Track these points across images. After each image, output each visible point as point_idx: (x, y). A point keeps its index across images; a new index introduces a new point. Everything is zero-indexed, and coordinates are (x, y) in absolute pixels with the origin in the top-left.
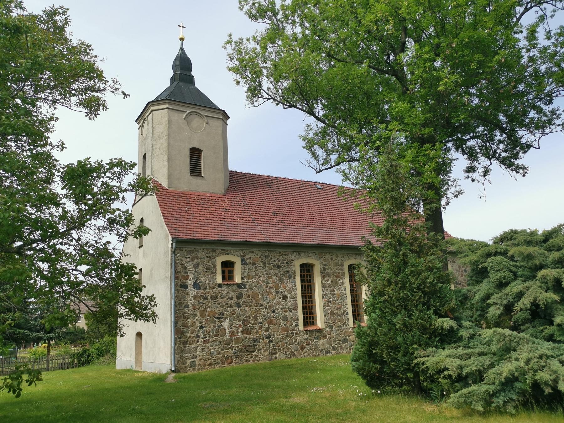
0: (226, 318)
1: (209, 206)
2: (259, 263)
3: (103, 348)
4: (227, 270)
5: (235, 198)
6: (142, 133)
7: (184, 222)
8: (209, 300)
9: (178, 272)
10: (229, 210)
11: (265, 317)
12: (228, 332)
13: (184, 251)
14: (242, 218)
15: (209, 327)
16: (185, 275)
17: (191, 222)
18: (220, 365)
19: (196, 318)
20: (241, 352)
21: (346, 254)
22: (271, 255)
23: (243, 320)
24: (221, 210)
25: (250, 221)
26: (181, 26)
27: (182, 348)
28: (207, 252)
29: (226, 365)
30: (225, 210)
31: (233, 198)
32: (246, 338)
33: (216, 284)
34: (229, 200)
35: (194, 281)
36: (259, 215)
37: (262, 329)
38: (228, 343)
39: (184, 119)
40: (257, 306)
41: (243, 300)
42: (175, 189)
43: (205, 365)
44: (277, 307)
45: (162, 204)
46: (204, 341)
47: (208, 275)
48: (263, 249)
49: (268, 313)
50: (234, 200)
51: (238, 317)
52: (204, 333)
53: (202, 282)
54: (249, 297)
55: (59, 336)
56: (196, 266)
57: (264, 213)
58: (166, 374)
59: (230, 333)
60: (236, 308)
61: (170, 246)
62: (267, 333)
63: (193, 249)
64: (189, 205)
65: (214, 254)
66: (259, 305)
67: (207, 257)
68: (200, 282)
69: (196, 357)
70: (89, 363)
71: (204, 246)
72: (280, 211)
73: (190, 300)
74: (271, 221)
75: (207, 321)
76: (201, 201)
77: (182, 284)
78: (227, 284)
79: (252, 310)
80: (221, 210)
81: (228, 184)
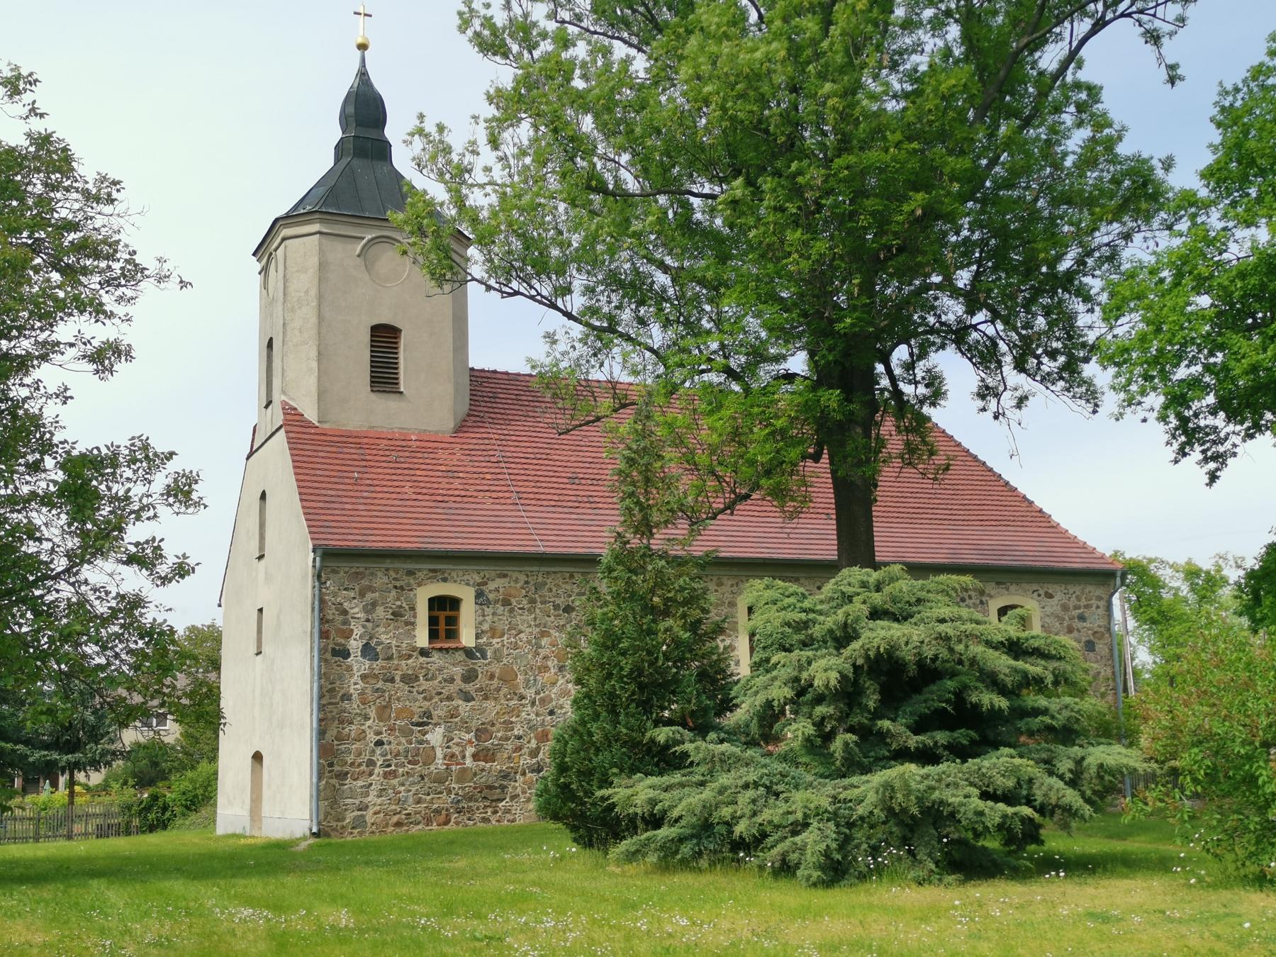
0: (436, 725)
1: (411, 466)
2: (519, 601)
3: (198, 791)
4: (442, 615)
5: (481, 441)
6: (265, 285)
7: (347, 506)
9: (328, 621)
10: (461, 475)
11: (531, 724)
12: (441, 756)
13: (342, 574)
14: (488, 494)
15: (398, 743)
16: (345, 627)
18: (420, 827)
19: (369, 723)
20: (471, 799)
21: (744, 579)
22: (548, 581)
23: (477, 730)
24: (440, 474)
26: (360, 14)
27: (334, 786)
28: (394, 576)
29: (434, 827)
30: (450, 474)
32: (483, 770)
33: (414, 649)
34: (465, 447)
35: (365, 641)
36: (533, 484)
37: (523, 751)
38: (440, 780)
39: (359, 256)
40: (511, 699)
41: (477, 684)
42: (334, 426)
43: (387, 825)
44: (560, 702)
45: (299, 464)
46: (385, 773)
47: (397, 628)
48: (531, 569)
49: (537, 715)
50: (477, 447)
51: (466, 723)
52: (386, 755)
54: (492, 677)
55: (95, 760)
56: (371, 608)
57: (547, 479)
58: (300, 839)
59: (444, 758)
60: (460, 702)
61: (310, 563)
62: (534, 760)
64: (364, 463)
65: (412, 581)
66: (516, 697)
67: (395, 587)
68: (379, 644)
69: (367, 807)
70: (165, 827)
71: (388, 564)
72: (590, 471)
73: (355, 684)
74: (562, 498)
75: (391, 729)
76: (393, 453)
77: (337, 648)
78: (441, 649)
79: (498, 707)
80: (440, 474)
81: (464, 407)
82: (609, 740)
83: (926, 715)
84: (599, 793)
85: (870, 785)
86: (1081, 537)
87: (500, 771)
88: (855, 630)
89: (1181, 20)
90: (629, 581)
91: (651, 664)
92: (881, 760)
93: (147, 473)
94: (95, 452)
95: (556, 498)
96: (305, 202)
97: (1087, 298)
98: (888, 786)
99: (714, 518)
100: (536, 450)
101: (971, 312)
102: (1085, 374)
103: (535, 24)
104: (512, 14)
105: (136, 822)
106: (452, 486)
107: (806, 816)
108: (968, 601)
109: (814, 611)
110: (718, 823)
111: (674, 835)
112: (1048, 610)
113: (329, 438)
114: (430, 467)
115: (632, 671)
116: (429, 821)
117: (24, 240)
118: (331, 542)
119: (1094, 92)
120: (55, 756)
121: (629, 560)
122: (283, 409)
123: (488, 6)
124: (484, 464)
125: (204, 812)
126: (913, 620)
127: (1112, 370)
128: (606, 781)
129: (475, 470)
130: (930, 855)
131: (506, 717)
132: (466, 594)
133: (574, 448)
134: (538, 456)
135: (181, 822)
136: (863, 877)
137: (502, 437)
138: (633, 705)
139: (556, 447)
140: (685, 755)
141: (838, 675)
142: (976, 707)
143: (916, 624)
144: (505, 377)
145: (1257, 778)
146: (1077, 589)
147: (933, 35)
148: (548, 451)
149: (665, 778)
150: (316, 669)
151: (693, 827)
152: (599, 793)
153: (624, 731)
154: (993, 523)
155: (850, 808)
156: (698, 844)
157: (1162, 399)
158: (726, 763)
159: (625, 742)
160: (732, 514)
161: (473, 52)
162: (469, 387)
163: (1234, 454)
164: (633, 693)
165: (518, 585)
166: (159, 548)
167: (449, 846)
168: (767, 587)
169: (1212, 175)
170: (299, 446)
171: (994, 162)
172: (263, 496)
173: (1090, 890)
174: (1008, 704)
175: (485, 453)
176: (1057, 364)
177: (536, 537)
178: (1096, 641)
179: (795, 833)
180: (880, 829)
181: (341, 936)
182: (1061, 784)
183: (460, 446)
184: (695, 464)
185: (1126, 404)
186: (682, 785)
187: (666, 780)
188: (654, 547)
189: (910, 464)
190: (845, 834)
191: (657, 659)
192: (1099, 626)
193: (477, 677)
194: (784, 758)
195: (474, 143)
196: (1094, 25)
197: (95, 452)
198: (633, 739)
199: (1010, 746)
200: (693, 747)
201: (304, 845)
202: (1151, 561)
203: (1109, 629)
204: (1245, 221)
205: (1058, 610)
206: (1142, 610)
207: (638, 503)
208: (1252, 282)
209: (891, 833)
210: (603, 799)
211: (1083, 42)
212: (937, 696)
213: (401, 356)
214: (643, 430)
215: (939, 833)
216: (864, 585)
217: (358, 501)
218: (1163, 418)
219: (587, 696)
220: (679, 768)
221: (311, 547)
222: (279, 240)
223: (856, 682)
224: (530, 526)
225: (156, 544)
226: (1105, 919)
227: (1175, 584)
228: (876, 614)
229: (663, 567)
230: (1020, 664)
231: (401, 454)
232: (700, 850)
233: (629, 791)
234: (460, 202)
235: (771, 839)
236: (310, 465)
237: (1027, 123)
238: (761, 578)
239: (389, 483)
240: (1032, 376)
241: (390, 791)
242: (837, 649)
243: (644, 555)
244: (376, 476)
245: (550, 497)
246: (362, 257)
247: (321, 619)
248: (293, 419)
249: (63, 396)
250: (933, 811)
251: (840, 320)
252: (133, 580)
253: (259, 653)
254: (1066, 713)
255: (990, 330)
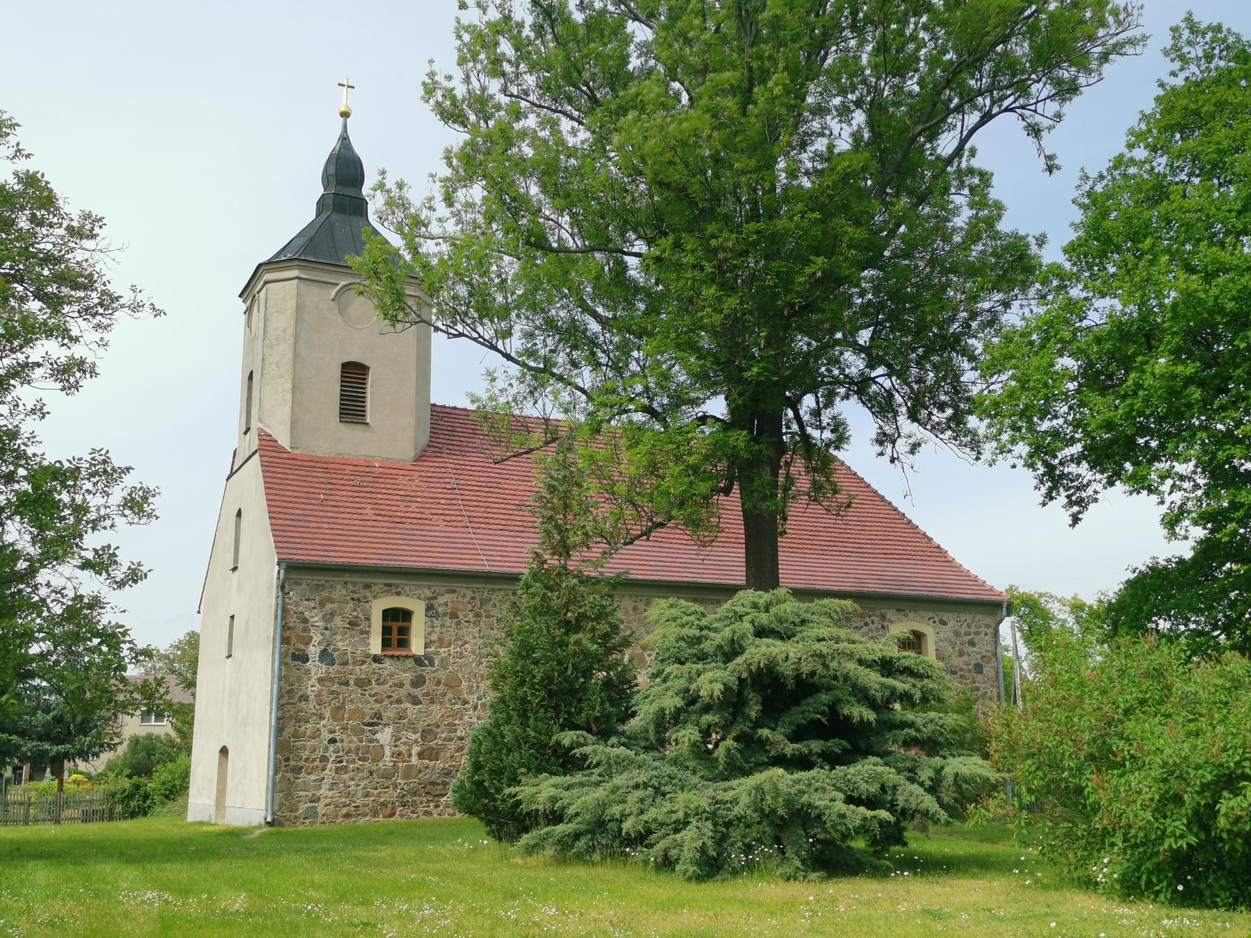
0: (385, 725)
1: (373, 490)
2: (466, 615)
4: (395, 626)
5: (438, 470)
6: (249, 324)
7: (312, 525)
8: (352, 687)
9: (289, 628)
12: (389, 754)
13: (304, 586)
14: (442, 517)
15: (350, 741)
16: (305, 634)
17: (326, 526)
18: (367, 818)
19: (324, 722)
20: (415, 794)
22: (493, 597)
24: (399, 498)
25: (460, 524)
29: (381, 818)
30: (409, 499)
31: (433, 470)
32: (427, 767)
33: (368, 656)
34: (423, 474)
35: (322, 648)
38: (387, 775)
39: (333, 300)
40: (455, 704)
42: (305, 452)
43: (337, 816)
45: (270, 486)
46: (337, 768)
48: (476, 586)
49: (479, 718)
50: (434, 475)
52: (338, 752)
53: (339, 650)
54: (438, 683)
55: (83, 751)
57: (497, 505)
58: (255, 827)
60: (409, 705)
61: (275, 576)
63: (322, 582)
65: (368, 594)
66: (460, 702)
67: (353, 599)
68: (335, 650)
70: (145, 814)
71: (346, 578)
73: (313, 686)
74: (509, 522)
75: (344, 728)
76: (357, 478)
78: (392, 657)
79: (443, 710)
80: (399, 498)
81: (425, 439)
82: (519, 742)
83: (803, 724)
84: (507, 791)
85: (742, 788)
86: (973, 572)
87: (443, 769)
88: (741, 646)
89: (1058, 117)
90: (544, 597)
91: (561, 673)
92: (761, 765)
93: (106, 486)
94: (58, 465)
95: (504, 522)
96: (287, 250)
97: (972, 358)
98: (759, 788)
99: (631, 543)
100: (488, 479)
101: (872, 367)
102: (969, 425)
103: (491, 97)
104: (470, 87)
105: (119, 808)
106: (409, 509)
107: (687, 815)
108: (871, 625)
109: (709, 629)
110: (610, 821)
111: (570, 830)
112: (942, 635)
113: (299, 463)
114: (390, 491)
115: (543, 680)
116: (375, 814)
117: (7, 271)
118: (295, 557)
119: (985, 177)
120: (47, 746)
121: (547, 579)
122: (259, 435)
123: (449, 78)
124: (441, 490)
125: (180, 801)
126: (795, 639)
127: (987, 421)
128: (515, 780)
129: (431, 495)
130: (797, 854)
131: (450, 720)
132: (417, 607)
133: (522, 478)
134: (490, 485)
135: (159, 809)
136: (735, 873)
137: (458, 467)
138: (542, 710)
139: (507, 477)
140: (585, 757)
141: (722, 687)
142: (848, 718)
143: (798, 642)
144: (464, 413)
145: (1083, 789)
146: (969, 618)
147: (841, 121)
148: (499, 480)
149: (568, 777)
150: (276, 671)
151: (589, 823)
152: (507, 791)
153: (533, 734)
154: (895, 556)
155: (729, 809)
156: (592, 839)
157: (1027, 449)
158: (622, 765)
159: (534, 744)
160: (648, 539)
161: (435, 120)
162: (429, 421)
163: (1096, 500)
164: (543, 700)
165: (465, 600)
166: (114, 555)
167: (388, 836)
168: (671, 606)
169: (1074, 250)
170: (272, 469)
171: (892, 233)
172: (239, 514)
173: (938, 889)
174: (875, 716)
175: (441, 480)
176: (945, 415)
177: (483, 558)
178: (984, 664)
179: (677, 831)
180: (755, 828)
181: (227, 919)
182: (921, 790)
183: (419, 474)
184: (613, 493)
185: (998, 451)
186: (582, 785)
187: (568, 779)
188: (570, 568)
189: (815, 500)
190: (722, 832)
191: (566, 669)
192: (987, 651)
193: (425, 683)
194: (675, 762)
195: (431, 199)
196: (982, 118)
197: (58, 465)
198: (540, 742)
199: (878, 755)
200: (594, 749)
201: (258, 832)
202: (1041, 595)
203: (996, 654)
204: (1100, 292)
205: (951, 635)
206: (1033, 639)
207: (557, 527)
208: (1107, 347)
209: (765, 832)
210: (511, 796)
211: (972, 132)
212: (813, 709)
213: (369, 391)
214: (564, 461)
215: (807, 834)
216: (755, 606)
217: (322, 520)
218: (1031, 466)
219: (502, 700)
220: (582, 769)
221: (276, 560)
222: (262, 283)
223: (740, 693)
224: (478, 547)
225: (111, 552)
226: (936, 916)
227: (1061, 616)
228: (761, 632)
229: (575, 584)
230: (890, 681)
231: (364, 479)
232: (593, 845)
233: (534, 790)
234: (415, 250)
235: (655, 836)
236: (280, 487)
237: (922, 199)
238: (667, 598)
239: (352, 505)
240: (924, 425)
241: (341, 785)
242: (725, 663)
243: (559, 574)
244: (340, 498)
245: (498, 522)
246: (336, 301)
247: (284, 626)
248: (267, 446)
249: (39, 411)
250: (802, 813)
251: (748, 369)
252: (90, 584)
253: (229, 656)
254: (931, 727)
255: (887, 384)
